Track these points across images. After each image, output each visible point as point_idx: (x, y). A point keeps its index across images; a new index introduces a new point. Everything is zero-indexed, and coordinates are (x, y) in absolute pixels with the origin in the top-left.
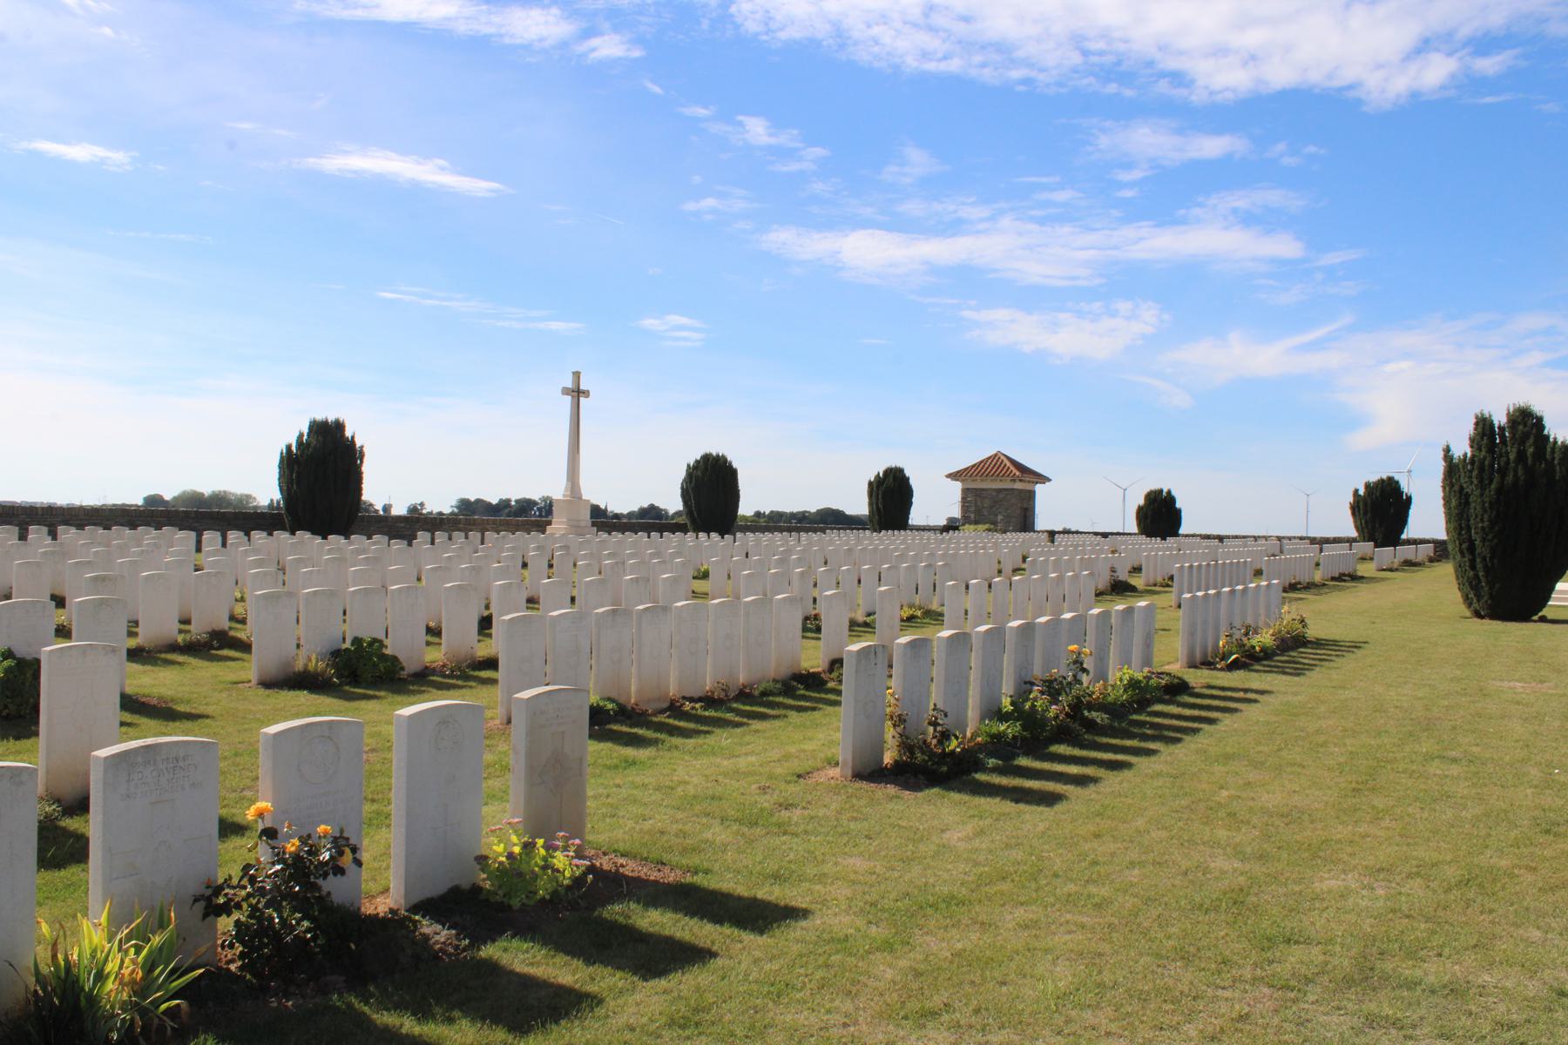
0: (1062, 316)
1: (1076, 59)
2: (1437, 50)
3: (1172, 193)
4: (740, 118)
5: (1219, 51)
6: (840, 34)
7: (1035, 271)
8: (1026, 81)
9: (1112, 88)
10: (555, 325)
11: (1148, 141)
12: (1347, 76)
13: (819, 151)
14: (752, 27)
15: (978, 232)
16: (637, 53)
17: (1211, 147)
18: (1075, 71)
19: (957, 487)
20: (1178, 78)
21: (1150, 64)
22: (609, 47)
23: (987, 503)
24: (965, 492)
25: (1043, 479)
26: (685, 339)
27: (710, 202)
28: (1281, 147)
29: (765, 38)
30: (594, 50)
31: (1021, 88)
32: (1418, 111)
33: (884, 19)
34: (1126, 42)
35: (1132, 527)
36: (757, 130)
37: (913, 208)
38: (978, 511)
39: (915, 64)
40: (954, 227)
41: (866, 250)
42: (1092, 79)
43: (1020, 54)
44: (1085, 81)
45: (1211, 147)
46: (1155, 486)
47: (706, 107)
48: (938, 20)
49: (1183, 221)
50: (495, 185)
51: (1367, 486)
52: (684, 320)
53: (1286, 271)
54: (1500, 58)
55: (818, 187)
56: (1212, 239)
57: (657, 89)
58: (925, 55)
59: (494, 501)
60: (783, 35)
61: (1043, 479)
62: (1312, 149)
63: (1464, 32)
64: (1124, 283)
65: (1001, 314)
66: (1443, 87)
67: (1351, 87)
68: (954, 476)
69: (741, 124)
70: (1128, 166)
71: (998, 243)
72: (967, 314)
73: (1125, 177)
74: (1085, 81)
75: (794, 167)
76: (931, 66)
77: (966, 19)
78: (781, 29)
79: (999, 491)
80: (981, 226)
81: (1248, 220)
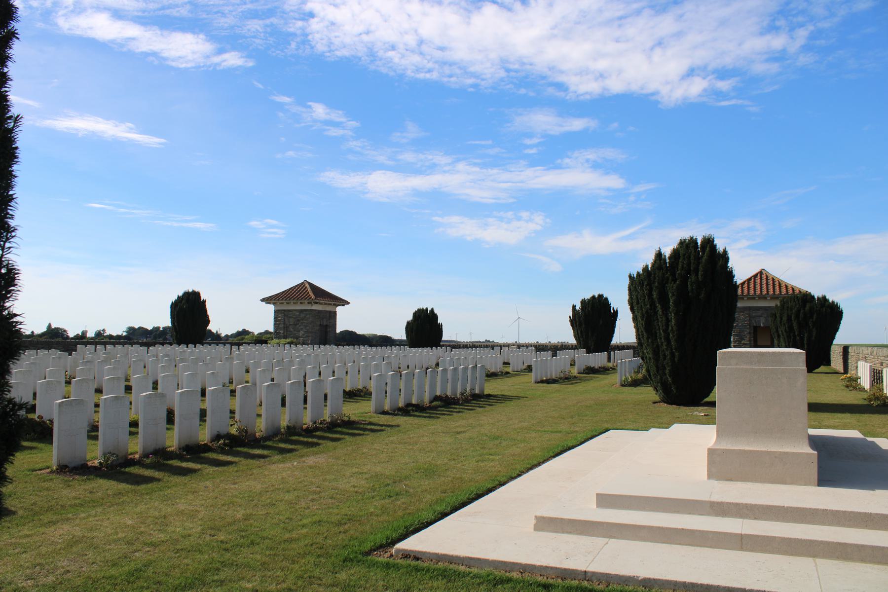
0: (490, 220)
1: (503, 74)
2: (698, 75)
3: (553, 152)
4: (310, 103)
5: (583, 72)
6: (372, 53)
7: (477, 194)
8: (475, 86)
9: (523, 91)
10: (199, 225)
11: (543, 121)
12: (652, 87)
13: (353, 124)
14: (320, 48)
15: (445, 172)
16: (251, 64)
17: (577, 124)
18: (502, 80)
19: (271, 308)
20: (561, 87)
21: (544, 78)
22: (232, 59)
23: (292, 321)
24: (277, 312)
25: (344, 302)
26: (275, 233)
27: (291, 153)
28: (615, 125)
29: (328, 54)
30: (224, 61)
31: (472, 90)
32: (689, 110)
33: (393, 48)
34: (531, 65)
35: (568, 336)
36: (320, 111)
37: (408, 157)
38: (286, 328)
39: (413, 74)
40: (432, 168)
41: (382, 184)
42: (511, 86)
43: (472, 69)
44: (508, 87)
45: (577, 124)
46: (423, 306)
47: (289, 97)
48: (424, 48)
49: (559, 167)
50: (163, 140)
51: (583, 302)
52: (274, 222)
53: (617, 195)
54: (729, 82)
55: (354, 144)
56: (577, 176)
57: (260, 86)
58: (418, 70)
59: (150, 328)
60: (338, 53)
61: (344, 302)
62: (632, 128)
63: (710, 68)
64: (527, 201)
65: (455, 219)
66: (699, 95)
67: (653, 94)
68: (268, 300)
69: (310, 107)
70: (530, 135)
71: (458, 178)
72: (436, 218)
73: (528, 142)
74: (508, 87)
75: (340, 132)
76: (421, 76)
77: (442, 49)
78: (337, 50)
79: (301, 311)
80: (446, 168)
81: (595, 166)
